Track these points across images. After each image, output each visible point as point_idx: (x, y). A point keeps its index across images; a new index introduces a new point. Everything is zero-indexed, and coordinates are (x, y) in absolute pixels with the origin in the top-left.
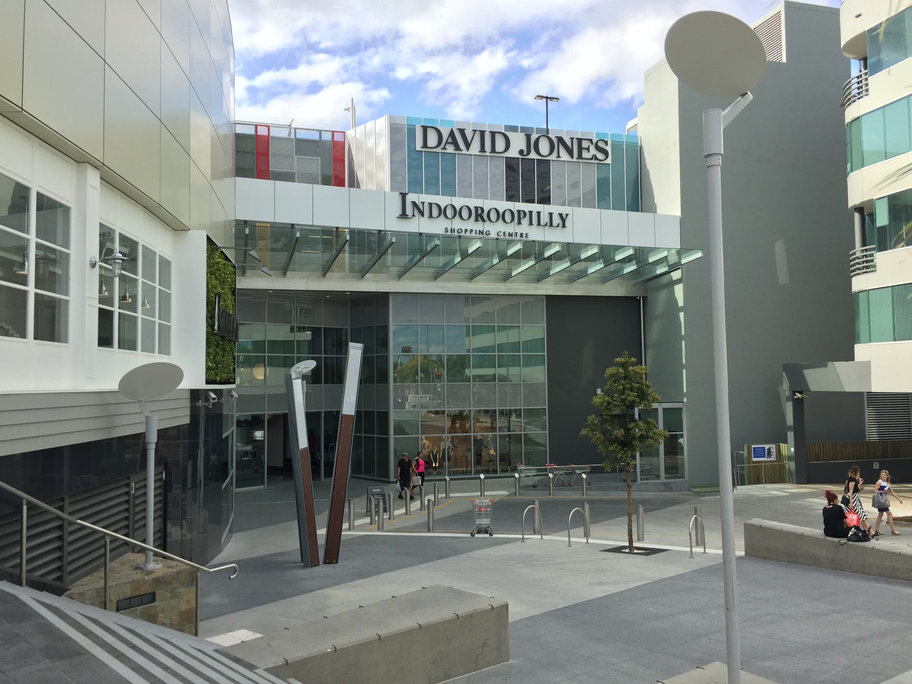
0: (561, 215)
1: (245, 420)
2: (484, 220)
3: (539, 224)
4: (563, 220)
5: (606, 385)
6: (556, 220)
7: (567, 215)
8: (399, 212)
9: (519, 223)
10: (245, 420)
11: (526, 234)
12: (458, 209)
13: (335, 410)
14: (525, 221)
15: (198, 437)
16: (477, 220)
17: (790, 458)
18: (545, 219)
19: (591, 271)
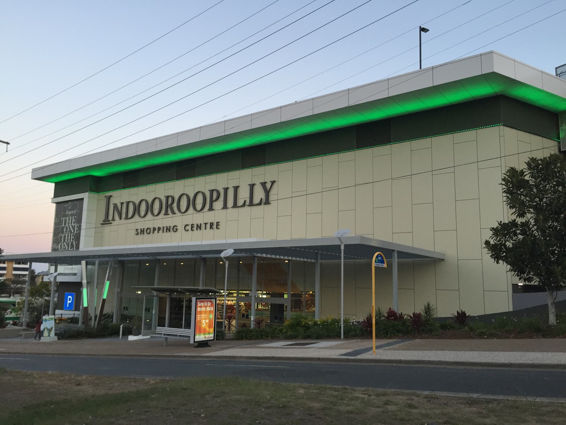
0: (264, 184)
1: (500, 224)
2: (173, 213)
3: (235, 206)
4: (267, 192)
5: (546, 187)
6: (259, 194)
7: (273, 182)
8: (103, 218)
9: (211, 209)
10: (500, 224)
11: (217, 223)
12: (191, 208)
13: (166, 328)
14: (218, 205)
15: (344, 262)
16: (166, 214)
17: (507, 195)
18: (244, 195)
19: (202, 416)
